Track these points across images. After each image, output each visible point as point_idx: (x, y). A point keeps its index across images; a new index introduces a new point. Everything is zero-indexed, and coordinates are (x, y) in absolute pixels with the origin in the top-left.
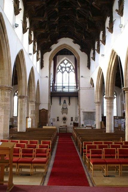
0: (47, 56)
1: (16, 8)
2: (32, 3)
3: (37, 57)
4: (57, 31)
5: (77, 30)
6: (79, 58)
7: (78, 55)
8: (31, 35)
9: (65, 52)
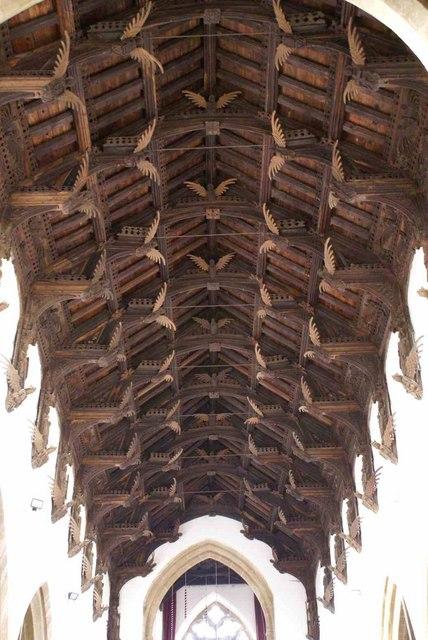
0: (137, 592)
1: (39, 448)
2: (91, 414)
3: (95, 601)
4: (175, 495)
5: (255, 489)
6: (271, 599)
7: (265, 585)
8: (78, 521)
9: (211, 572)
